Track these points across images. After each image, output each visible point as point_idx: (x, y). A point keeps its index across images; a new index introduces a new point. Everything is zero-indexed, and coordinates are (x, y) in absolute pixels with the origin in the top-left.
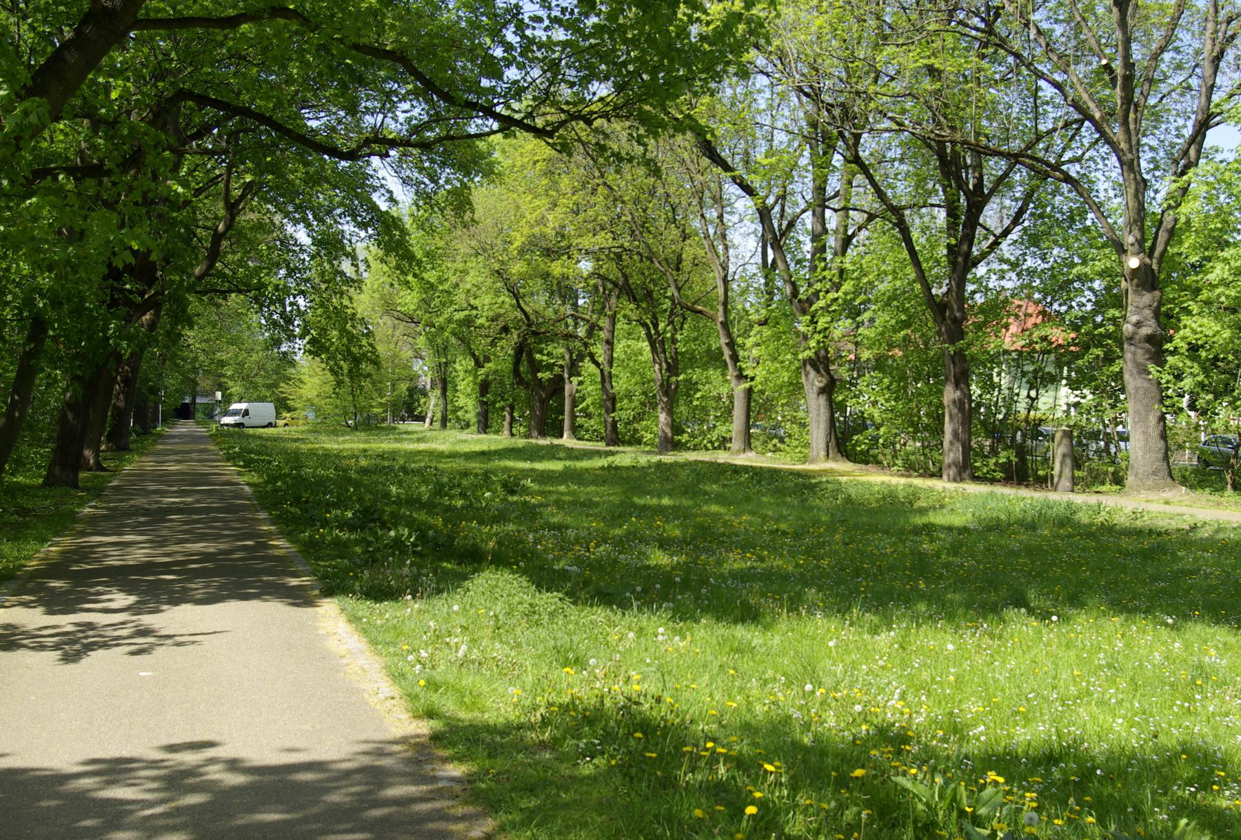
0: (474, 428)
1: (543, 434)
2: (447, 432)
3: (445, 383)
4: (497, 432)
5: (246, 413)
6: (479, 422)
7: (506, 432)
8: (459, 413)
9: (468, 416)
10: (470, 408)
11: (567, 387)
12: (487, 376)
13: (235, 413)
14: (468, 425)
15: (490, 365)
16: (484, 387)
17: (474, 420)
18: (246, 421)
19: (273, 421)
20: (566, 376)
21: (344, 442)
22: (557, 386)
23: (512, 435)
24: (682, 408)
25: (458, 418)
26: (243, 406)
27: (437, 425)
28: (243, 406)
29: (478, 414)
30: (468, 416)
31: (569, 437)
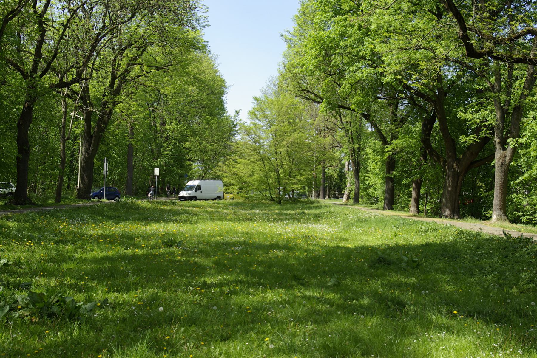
0: (381, 204)
1: (459, 212)
2: (357, 207)
3: (358, 166)
4: (402, 209)
5: (198, 188)
6: (385, 198)
7: (413, 209)
8: (370, 191)
9: (376, 193)
10: (379, 186)
11: (498, 154)
12: (395, 153)
13: (191, 188)
14: (377, 201)
15: (397, 141)
16: (390, 164)
17: (381, 197)
18: (198, 194)
19: (221, 195)
20: (496, 140)
21: (164, 204)
22: (482, 154)
23: (419, 211)
24: (190, 88)
25: (368, 194)
26: (196, 183)
27: (351, 201)
28: (196, 183)
29: (384, 192)
30: (376, 193)
31: (499, 219)
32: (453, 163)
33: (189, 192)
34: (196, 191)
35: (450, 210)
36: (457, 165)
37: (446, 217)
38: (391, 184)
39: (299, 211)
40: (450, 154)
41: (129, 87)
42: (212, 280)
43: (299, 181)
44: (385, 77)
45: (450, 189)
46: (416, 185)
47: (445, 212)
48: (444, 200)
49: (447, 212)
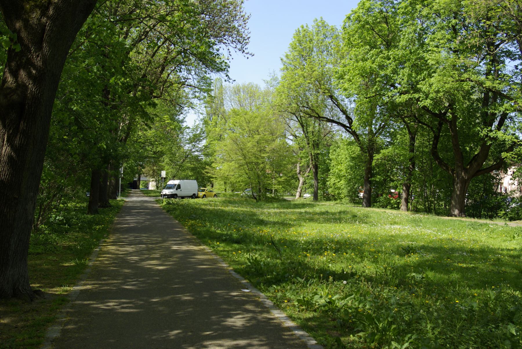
5: (179, 187)
18: (178, 192)
19: (196, 193)
32: (462, 171)
33: (171, 190)
34: (177, 189)
35: (459, 210)
36: (464, 173)
37: (455, 216)
38: (369, 185)
39: (216, 208)
40: (460, 164)
41: (318, 110)
42: (408, 260)
43: (279, 182)
44: (421, 101)
45: (458, 193)
46: (406, 188)
47: (454, 211)
48: (453, 202)
49: (456, 212)
